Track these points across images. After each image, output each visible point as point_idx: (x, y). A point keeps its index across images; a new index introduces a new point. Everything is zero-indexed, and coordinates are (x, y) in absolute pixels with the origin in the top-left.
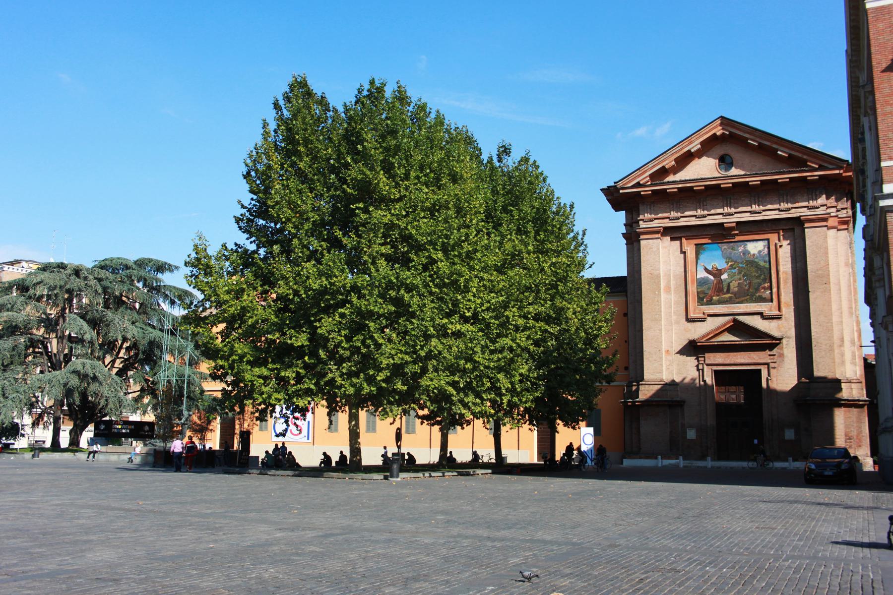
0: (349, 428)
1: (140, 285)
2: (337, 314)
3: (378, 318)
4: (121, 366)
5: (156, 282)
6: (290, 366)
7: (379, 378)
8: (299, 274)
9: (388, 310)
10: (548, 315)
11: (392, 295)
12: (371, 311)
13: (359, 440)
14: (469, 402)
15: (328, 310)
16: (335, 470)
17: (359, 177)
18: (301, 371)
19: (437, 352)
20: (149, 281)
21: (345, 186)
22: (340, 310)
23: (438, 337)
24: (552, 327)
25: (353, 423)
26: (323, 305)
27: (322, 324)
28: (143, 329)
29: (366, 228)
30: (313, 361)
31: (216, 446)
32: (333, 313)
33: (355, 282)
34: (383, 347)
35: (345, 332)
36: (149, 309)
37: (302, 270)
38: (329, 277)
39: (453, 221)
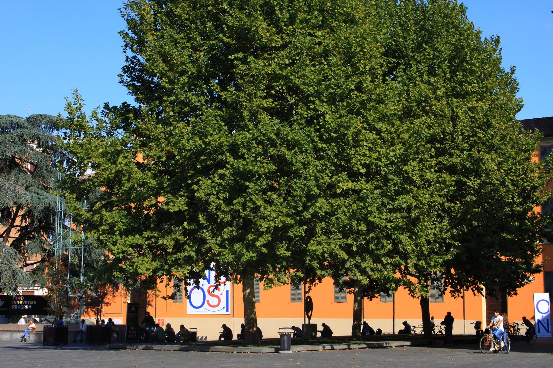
0: (244, 298)
1: (34, 145)
2: (216, 176)
3: (259, 179)
4: (17, 235)
5: (51, 141)
6: (169, 233)
7: (258, 244)
8: (171, 135)
9: (269, 169)
10: (464, 166)
11: (272, 153)
12: (250, 171)
13: (255, 310)
14: (365, 268)
15: (206, 172)
16: (236, 344)
17: (237, 24)
18: (179, 238)
19: (323, 214)
20: (43, 140)
21: (221, 35)
22: (220, 171)
23: (325, 197)
24: (471, 180)
25: (248, 291)
26: (199, 166)
27: (200, 186)
28: (38, 194)
29: (244, 80)
30: (193, 227)
31: (120, 320)
32: (213, 174)
33: (235, 140)
34: (262, 209)
35: (224, 195)
36: (45, 171)
37: (174, 130)
38: (202, 135)
39: (339, 69)
